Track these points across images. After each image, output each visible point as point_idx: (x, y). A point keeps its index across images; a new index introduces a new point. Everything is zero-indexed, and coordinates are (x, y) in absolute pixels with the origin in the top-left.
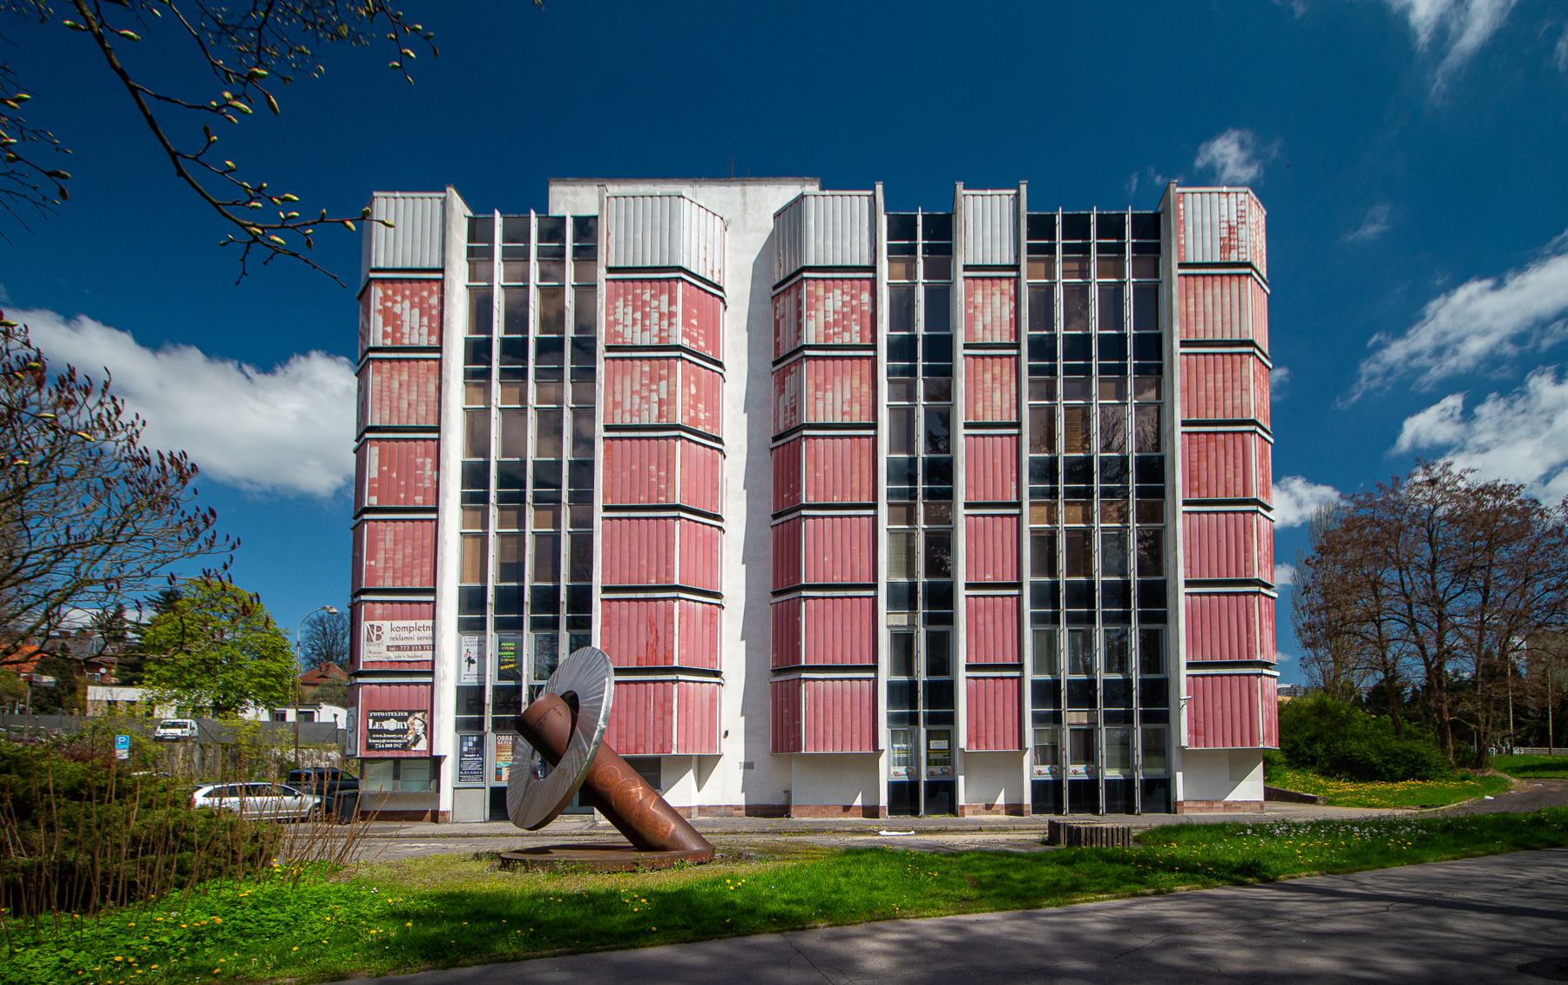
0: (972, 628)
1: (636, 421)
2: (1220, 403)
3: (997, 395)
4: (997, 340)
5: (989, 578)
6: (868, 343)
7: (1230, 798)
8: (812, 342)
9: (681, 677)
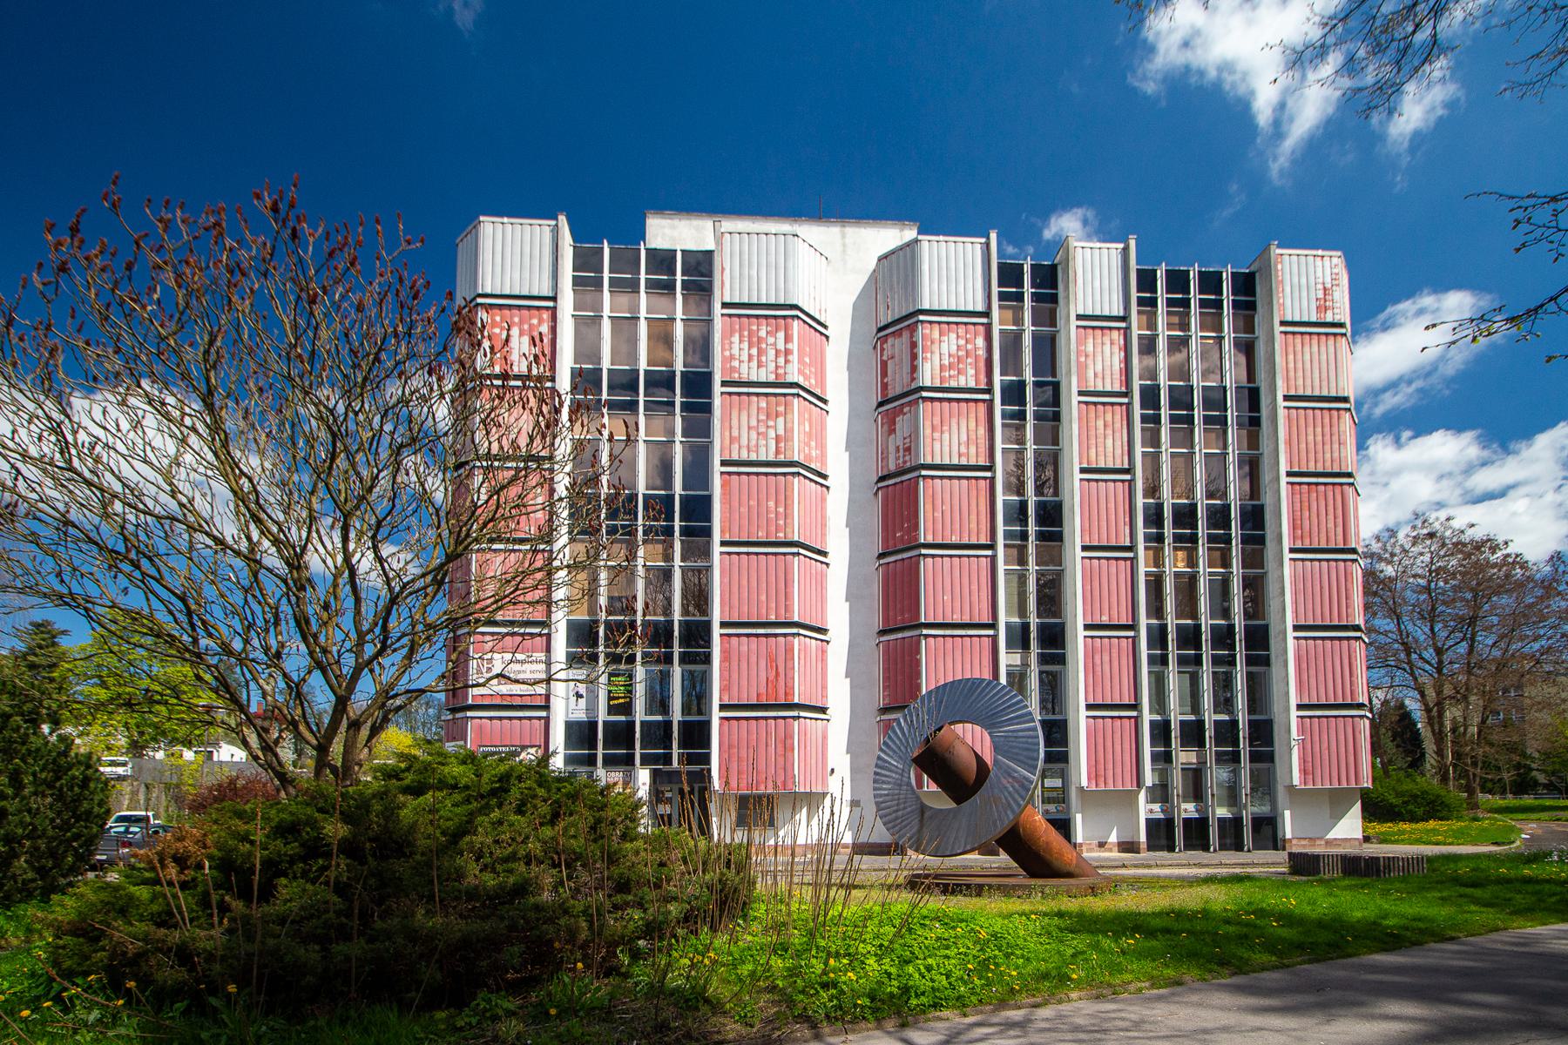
0: (1091, 668)
1: (753, 457)
2: (1320, 455)
3: (1109, 442)
4: (1108, 388)
5: (1105, 619)
6: (983, 387)
7: (1331, 836)
8: (928, 383)
9: (803, 714)
